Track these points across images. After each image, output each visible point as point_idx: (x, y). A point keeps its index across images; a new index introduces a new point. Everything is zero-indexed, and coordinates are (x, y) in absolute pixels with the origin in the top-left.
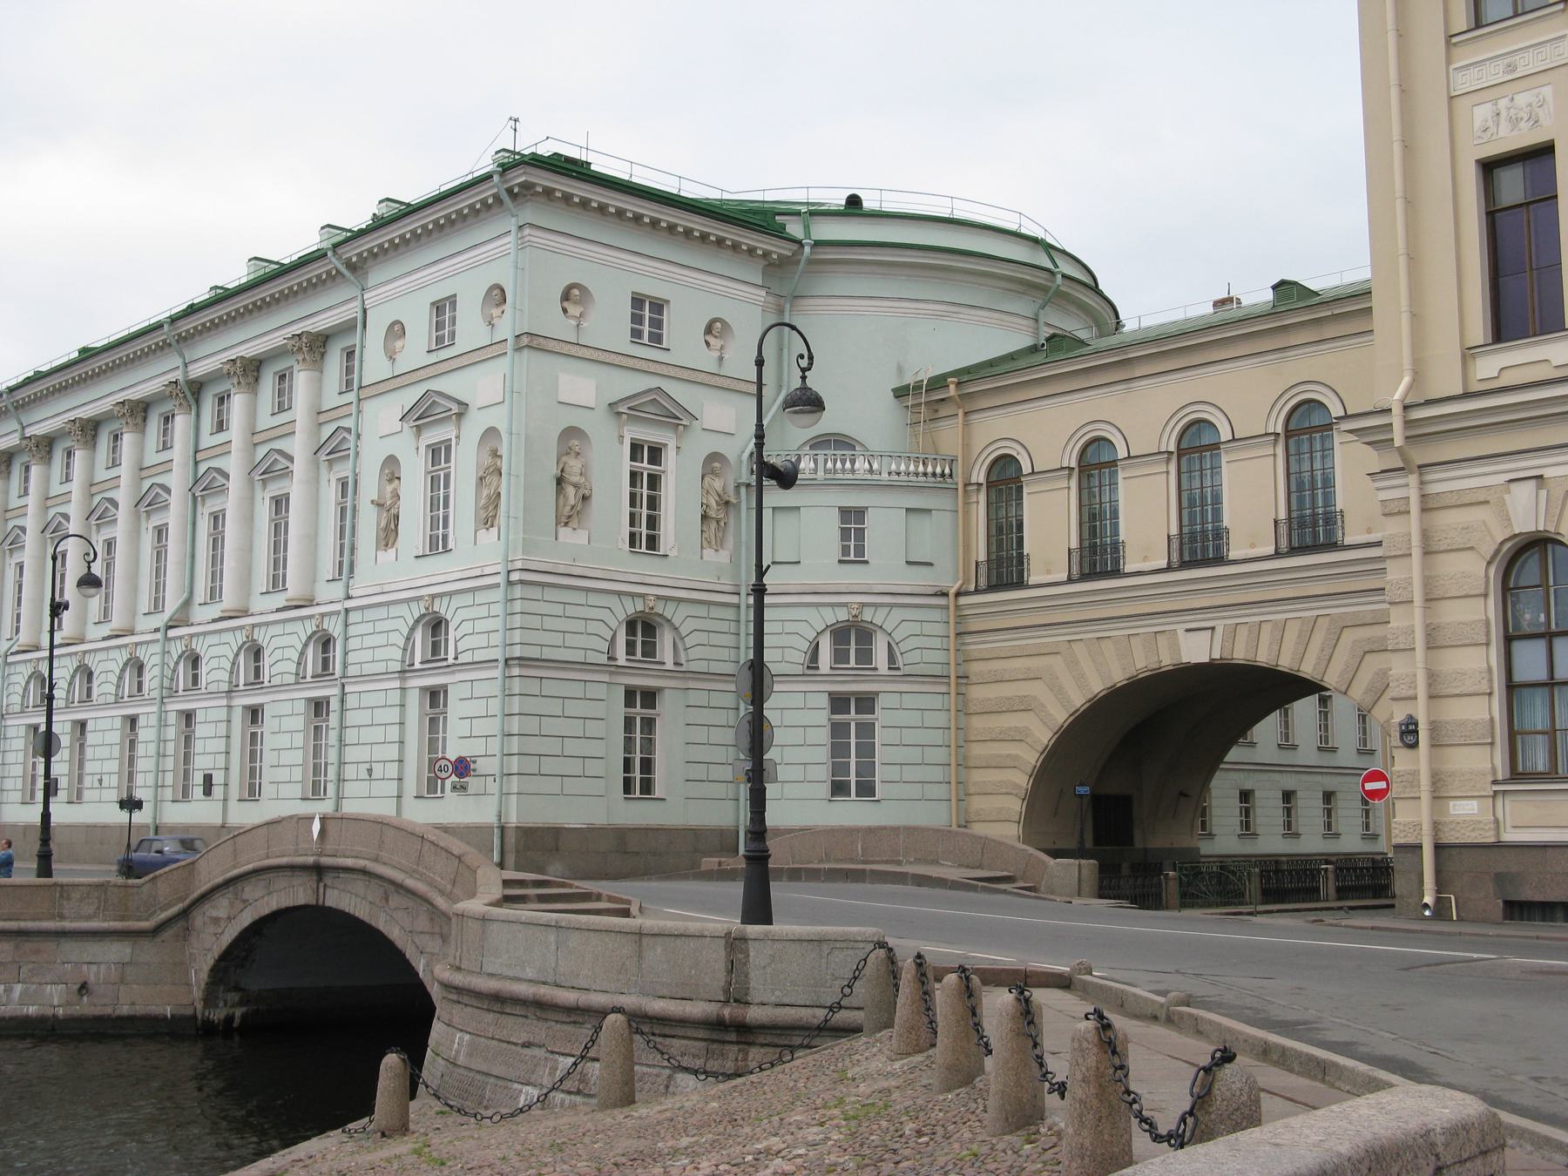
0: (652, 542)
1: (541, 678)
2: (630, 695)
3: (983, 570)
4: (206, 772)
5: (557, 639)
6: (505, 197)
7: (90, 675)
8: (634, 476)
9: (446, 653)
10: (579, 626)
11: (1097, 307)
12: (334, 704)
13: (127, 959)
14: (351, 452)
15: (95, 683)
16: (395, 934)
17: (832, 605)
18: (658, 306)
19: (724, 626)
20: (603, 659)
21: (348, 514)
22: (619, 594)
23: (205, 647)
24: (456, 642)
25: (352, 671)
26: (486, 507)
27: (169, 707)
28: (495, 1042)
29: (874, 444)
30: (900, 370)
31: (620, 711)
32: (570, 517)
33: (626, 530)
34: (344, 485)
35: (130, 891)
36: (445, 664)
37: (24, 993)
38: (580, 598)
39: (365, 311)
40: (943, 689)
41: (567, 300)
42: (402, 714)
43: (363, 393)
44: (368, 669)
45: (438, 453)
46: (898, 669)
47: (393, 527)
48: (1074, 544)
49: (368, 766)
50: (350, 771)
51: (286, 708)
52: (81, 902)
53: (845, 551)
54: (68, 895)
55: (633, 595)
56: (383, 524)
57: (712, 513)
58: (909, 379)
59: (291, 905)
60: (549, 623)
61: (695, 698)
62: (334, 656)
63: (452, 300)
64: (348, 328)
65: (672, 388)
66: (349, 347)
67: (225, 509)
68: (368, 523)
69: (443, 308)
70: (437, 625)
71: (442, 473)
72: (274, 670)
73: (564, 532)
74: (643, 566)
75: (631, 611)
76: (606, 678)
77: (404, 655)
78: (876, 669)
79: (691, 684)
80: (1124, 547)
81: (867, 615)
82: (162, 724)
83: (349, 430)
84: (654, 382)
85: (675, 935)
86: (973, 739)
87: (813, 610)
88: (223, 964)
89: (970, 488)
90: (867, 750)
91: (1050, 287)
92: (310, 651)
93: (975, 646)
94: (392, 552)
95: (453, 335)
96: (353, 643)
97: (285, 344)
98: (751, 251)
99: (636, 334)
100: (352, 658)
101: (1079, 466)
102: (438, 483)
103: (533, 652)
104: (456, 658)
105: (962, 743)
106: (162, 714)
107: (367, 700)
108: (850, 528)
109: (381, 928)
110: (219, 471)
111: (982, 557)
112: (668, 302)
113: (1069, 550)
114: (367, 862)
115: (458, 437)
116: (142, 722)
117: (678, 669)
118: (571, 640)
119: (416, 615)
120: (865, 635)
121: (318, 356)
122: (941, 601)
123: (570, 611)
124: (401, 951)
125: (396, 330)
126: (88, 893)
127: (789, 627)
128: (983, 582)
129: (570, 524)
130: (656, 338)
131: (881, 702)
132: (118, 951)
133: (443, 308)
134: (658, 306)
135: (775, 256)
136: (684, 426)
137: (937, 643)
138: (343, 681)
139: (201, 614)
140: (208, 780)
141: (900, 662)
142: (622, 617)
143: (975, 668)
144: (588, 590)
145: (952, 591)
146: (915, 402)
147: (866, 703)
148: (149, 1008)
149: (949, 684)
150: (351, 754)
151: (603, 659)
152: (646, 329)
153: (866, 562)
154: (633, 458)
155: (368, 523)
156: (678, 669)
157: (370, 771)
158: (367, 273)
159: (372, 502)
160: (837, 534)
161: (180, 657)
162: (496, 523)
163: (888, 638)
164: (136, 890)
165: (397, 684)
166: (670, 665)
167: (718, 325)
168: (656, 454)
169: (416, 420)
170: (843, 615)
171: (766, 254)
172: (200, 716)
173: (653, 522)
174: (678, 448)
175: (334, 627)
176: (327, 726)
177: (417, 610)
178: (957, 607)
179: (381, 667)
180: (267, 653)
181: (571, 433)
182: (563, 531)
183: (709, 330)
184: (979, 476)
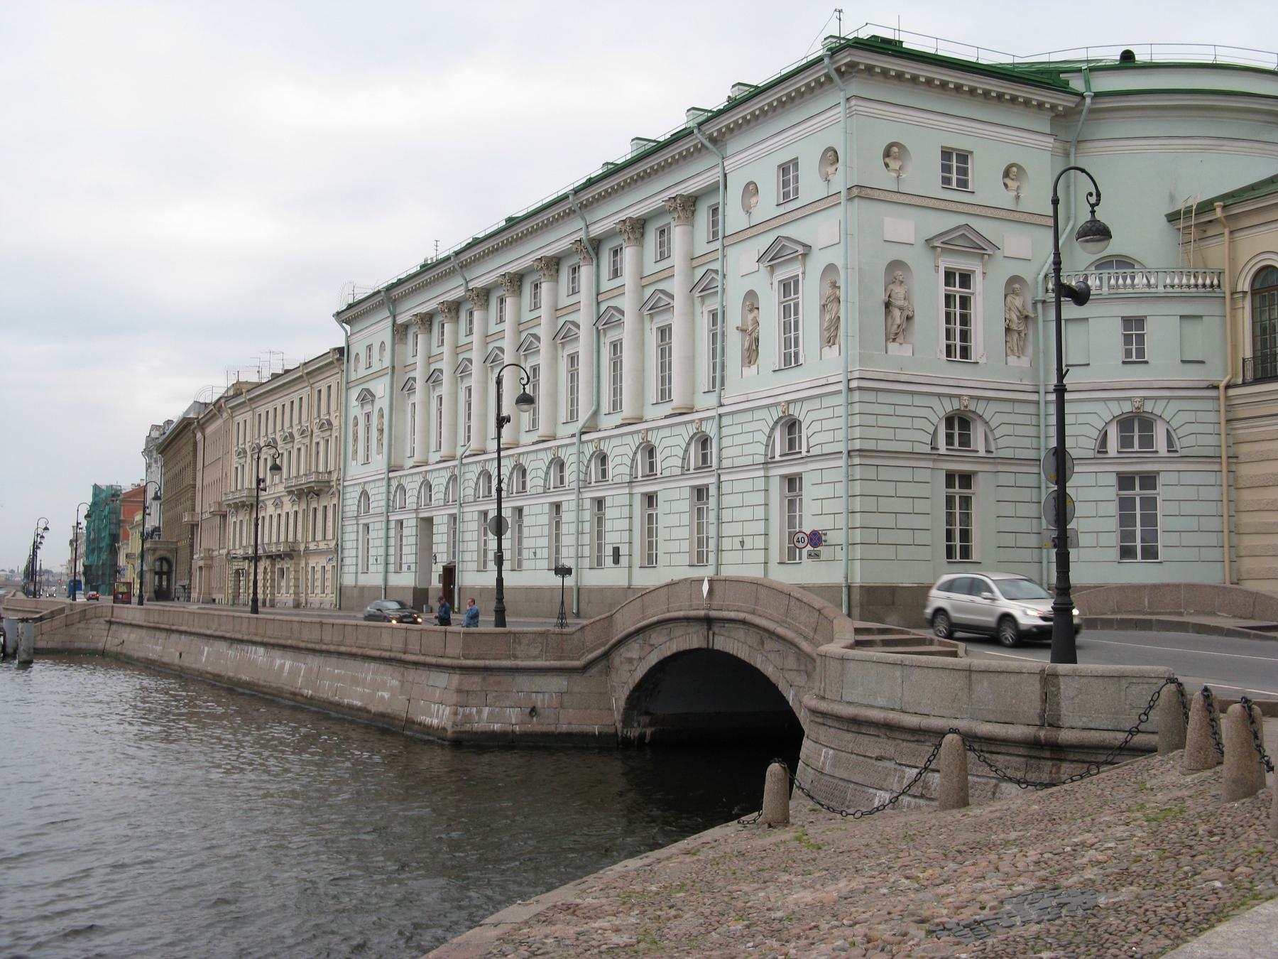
0: (965, 352)
1: (877, 466)
2: (950, 477)
3: (1249, 366)
4: (615, 546)
5: (889, 434)
6: (834, 75)
7: (524, 472)
8: (949, 299)
9: (800, 447)
10: (906, 422)
13: (565, 690)
14: (719, 289)
15: (528, 478)
16: (769, 671)
17: (1118, 399)
18: (963, 157)
20: (928, 449)
21: (717, 339)
22: (939, 395)
24: (808, 438)
25: (725, 463)
26: (828, 329)
29: (1151, 261)
30: (1172, 198)
32: (897, 334)
36: (799, 456)
37: (490, 714)
38: (907, 399)
39: (725, 175)
40: (1216, 467)
42: (767, 497)
44: (738, 462)
45: (788, 287)
46: (1176, 451)
47: (754, 347)
49: (740, 539)
50: (726, 544)
53: (1128, 353)
55: (951, 396)
56: (746, 345)
57: (1014, 327)
58: (1180, 206)
59: (688, 648)
60: (882, 421)
61: (1004, 479)
63: (795, 162)
64: (712, 189)
65: (976, 224)
68: (735, 345)
69: (788, 170)
70: (792, 425)
74: (958, 373)
75: (949, 409)
77: (766, 450)
78: (1157, 452)
79: (1000, 468)
81: (1148, 407)
82: (580, 508)
83: (716, 272)
84: (962, 220)
87: (1102, 404)
89: (1236, 296)
90: (1149, 520)
93: (1243, 430)
94: (754, 368)
95: (796, 190)
96: (725, 442)
97: (664, 205)
98: (1040, 105)
99: (946, 181)
100: (725, 453)
102: (789, 311)
103: (870, 445)
104: (808, 451)
105: (1233, 513)
106: (580, 500)
107: (738, 487)
108: (1132, 335)
109: (759, 667)
111: (1248, 354)
112: (971, 153)
115: (804, 273)
116: (564, 507)
117: (989, 455)
118: (901, 434)
120: (1147, 424)
121: (689, 214)
122: (1213, 393)
123: (900, 410)
125: (751, 189)
128: (1249, 376)
130: (963, 184)
131: (1161, 480)
133: (788, 170)
134: (963, 157)
136: (989, 255)
138: (719, 472)
139: (607, 422)
140: (616, 552)
141: (1177, 445)
142: (942, 414)
143: (1244, 449)
144: (913, 393)
145: (1222, 385)
146: (1186, 225)
147: (1149, 480)
149: (1221, 463)
150: (727, 530)
151: (928, 449)
152: (954, 176)
153: (1146, 362)
154: (947, 284)
155: (735, 345)
156: (989, 455)
157: (742, 543)
158: (726, 144)
159: (737, 328)
160: (1121, 339)
161: (592, 456)
162: (837, 341)
163: (1167, 426)
165: (762, 473)
166: (982, 453)
167: (1015, 169)
168: (966, 279)
170: (1127, 407)
171: (1053, 107)
172: (608, 502)
173: (965, 336)
174: (984, 273)
176: (707, 508)
178: (1227, 398)
179: (749, 460)
181: (895, 265)
184: (1245, 285)
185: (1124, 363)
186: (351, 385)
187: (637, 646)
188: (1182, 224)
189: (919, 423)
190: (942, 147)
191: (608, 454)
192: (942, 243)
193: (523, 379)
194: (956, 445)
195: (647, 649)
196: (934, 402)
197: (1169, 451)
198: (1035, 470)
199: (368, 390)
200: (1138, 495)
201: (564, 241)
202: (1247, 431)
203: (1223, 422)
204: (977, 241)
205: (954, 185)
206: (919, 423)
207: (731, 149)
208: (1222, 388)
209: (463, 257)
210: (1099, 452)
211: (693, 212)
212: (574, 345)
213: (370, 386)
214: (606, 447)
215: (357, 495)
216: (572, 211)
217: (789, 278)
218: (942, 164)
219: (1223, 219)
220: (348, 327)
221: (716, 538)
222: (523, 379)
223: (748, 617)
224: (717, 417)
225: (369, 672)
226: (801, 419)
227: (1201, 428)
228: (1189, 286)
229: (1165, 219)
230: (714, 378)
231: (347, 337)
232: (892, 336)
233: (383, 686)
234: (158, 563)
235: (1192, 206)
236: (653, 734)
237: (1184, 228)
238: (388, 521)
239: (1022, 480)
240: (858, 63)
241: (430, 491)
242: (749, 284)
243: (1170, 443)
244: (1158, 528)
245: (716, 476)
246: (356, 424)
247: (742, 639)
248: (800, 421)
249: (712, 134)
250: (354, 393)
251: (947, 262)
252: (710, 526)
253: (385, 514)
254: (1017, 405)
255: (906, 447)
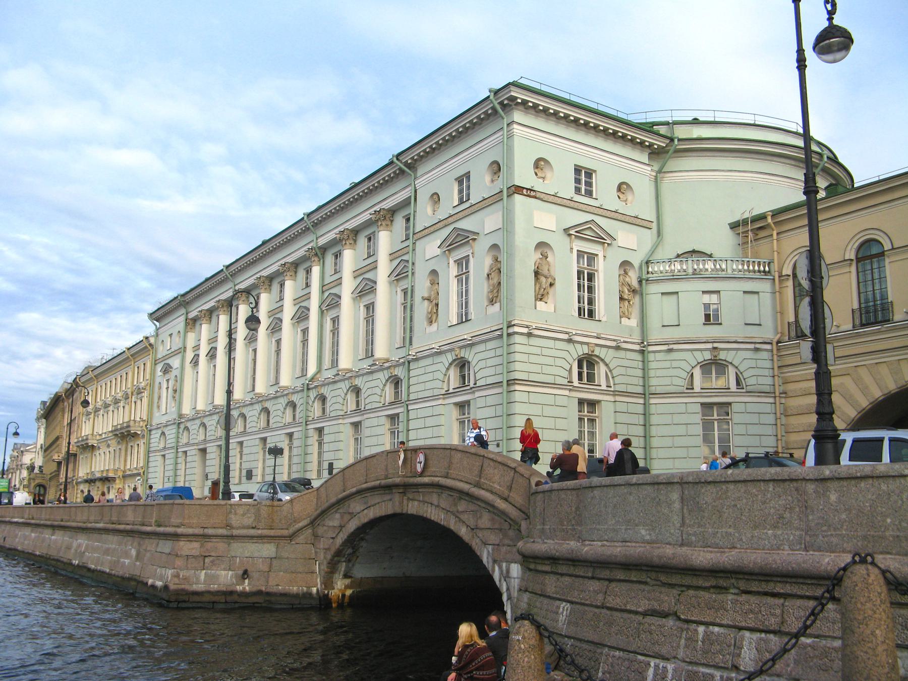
0: (591, 314)
2: (581, 402)
4: (330, 462)
6: (498, 107)
7: (269, 413)
8: (580, 273)
9: (469, 382)
10: (550, 361)
11: (842, 176)
12: (402, 418)
13: (273, 555)
14: (410, 273)
15: (271, 417)
18: (589, 174)
19: (635, 364)
20: (565, 382)
21: (408, 307)
22: (692, 350)
23: (329, 391)
24: (475, 374)
25: (412, 397)
26: (492, 291)
27: (309, 427)
28: (604, 611)
29: (717, 254)
31: (575, 414)
32: (543, 295)
33: (576, 305)
34: (405, 293)
35: (275, 509)
36: (468, 388)
38: (551, 343)
39: (416, 191)
41: (537, 168)
43: (416, 237)
44: (421, 395)
45: (463, 263)
48: (856, 306)
51: (375, 422)
52: (244, 516)
54: (235, 511)
55: (582, 343)
59: (383, 515)
60: (533, 359)
62: (401, 390)
63: (468, 175)
64: (406, 203)
65: (600, 220)
66: (406, 216)
67: (338, 316)
68: (422, 309)
69: (463, 180)
70: (462, 364)
71: (464, 277)
72: (367, 401)
73: (540, 304)
74: (586, 325)
75: (580, 353)
76: (566, 393)
80: (892, 305)
81: (722, 355)
83: (408, 261)
84: (589, 217)
85: (856, 478)
86: (791, 431)
88: (336, 559)
91: (819, 164)
92: (387, 388)
95: (468, 195)
96: (412, 381)
97: (371, 218)
98: (642, 143)
99: (578, 190)
100: (412, 389)
101: (857, 258)
104: (475, 384)
105: (784, 434)
107: (421, 413)
109: (452, 528)
110: (336, 295)
112: (595, 171)
113: (853, 310)
114: (440, 479)
116: (295, 436)
117: (609, 389)
118: (547, 370)
119: (450, 360)
121: (389, 223)
122: (768, 347)
123: (545, 351)
124: (467, 544)
125: (435, 198)
126: (248, 510)
127: (675, 364)
129: (543, 300)
130: (589, 193)
132: (268, 550)
133: (463, 180)
134: (589, 174)
135: (656, 147)
136: (608, 244)
137: (766, 372)
138: (407, 403)
142: (575, 356)
145: (775, 340)
146: (744, 230)
148: (206, 530)
151: (565, 382)
152: (583, 187)
155: (422, 309)
156: (609, 389)
158: (417, 170)
161: (315, 398)
163: (735, 370)
164: (279, 508)
166: (604, 387)
168: (592, 257)
169: (448, 246)
171: (651, 145)
172: (326, 431)
173: (591, 302)
175: (399, 372)
176: (398, 431)
177: (450, 357)
178: (778, 350)
180: (363, 391)
182: (538, 303)
183: (619, 189)
185: (704, 324)
186: (157, 362)
187: (337, 516)
188: (741, 229)
189: (560, 362)
190: (575, 165)
191: (327, 396)
192: (576, 232)
193: (251, 303)
194: (585, 381)
195: (347, 517)
196: (570, 347)
197: (737, 388)
198: (771, 400)
199: (168, 364)
200: (716, 420)
201: (301, 250)
202: (793, 374)
203: (776, 368)
204: (600, 234)
205: (583, 192)
206: (560, 362)
207: (420, 172)
208: (774, 344)
209: (232, 269)
210: (687, 389)
211: (392, 221)
212: (306, 322)
213: (169, 361)
214: (326, 391)
215: (158, 435)
216: (307, 229)
217: (462, 258)
218: (575, 178)
219: (773, 225)
220: (157, 324)
221: (405, 431)
222: (251, 303)
223: (443, 481)
224: (407, 363)
225: (112, 542)
226: (470, 360)
227: (760, 372)
228: (749, 271)
229: (728, 227)
230: (411, 310)
231: (157, 329)
232: (539, 296)
233: (127, 555)
234: (38, 488)
235: (748, 218)
236: (351, 596)
237: (743, 233)
238: (177, 452)
239: (632, 408)
240: (516, 98)
241: (206, 430)
242: (432, 265)
243: (738, 383)
244: (731, 444)
245: (406, 406)
246: (160, 388)
247: (436, 503)
248: (469, 362)
249: (407, 161)
250: (159, 367)
251: (579, 245)
252: (400, 433)
253: (175, 448)
254: (628, 353)
255: (550, 379)
